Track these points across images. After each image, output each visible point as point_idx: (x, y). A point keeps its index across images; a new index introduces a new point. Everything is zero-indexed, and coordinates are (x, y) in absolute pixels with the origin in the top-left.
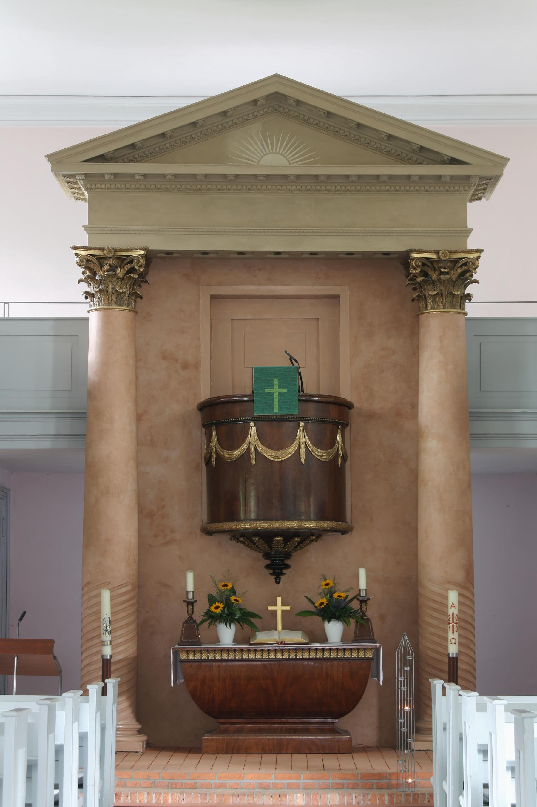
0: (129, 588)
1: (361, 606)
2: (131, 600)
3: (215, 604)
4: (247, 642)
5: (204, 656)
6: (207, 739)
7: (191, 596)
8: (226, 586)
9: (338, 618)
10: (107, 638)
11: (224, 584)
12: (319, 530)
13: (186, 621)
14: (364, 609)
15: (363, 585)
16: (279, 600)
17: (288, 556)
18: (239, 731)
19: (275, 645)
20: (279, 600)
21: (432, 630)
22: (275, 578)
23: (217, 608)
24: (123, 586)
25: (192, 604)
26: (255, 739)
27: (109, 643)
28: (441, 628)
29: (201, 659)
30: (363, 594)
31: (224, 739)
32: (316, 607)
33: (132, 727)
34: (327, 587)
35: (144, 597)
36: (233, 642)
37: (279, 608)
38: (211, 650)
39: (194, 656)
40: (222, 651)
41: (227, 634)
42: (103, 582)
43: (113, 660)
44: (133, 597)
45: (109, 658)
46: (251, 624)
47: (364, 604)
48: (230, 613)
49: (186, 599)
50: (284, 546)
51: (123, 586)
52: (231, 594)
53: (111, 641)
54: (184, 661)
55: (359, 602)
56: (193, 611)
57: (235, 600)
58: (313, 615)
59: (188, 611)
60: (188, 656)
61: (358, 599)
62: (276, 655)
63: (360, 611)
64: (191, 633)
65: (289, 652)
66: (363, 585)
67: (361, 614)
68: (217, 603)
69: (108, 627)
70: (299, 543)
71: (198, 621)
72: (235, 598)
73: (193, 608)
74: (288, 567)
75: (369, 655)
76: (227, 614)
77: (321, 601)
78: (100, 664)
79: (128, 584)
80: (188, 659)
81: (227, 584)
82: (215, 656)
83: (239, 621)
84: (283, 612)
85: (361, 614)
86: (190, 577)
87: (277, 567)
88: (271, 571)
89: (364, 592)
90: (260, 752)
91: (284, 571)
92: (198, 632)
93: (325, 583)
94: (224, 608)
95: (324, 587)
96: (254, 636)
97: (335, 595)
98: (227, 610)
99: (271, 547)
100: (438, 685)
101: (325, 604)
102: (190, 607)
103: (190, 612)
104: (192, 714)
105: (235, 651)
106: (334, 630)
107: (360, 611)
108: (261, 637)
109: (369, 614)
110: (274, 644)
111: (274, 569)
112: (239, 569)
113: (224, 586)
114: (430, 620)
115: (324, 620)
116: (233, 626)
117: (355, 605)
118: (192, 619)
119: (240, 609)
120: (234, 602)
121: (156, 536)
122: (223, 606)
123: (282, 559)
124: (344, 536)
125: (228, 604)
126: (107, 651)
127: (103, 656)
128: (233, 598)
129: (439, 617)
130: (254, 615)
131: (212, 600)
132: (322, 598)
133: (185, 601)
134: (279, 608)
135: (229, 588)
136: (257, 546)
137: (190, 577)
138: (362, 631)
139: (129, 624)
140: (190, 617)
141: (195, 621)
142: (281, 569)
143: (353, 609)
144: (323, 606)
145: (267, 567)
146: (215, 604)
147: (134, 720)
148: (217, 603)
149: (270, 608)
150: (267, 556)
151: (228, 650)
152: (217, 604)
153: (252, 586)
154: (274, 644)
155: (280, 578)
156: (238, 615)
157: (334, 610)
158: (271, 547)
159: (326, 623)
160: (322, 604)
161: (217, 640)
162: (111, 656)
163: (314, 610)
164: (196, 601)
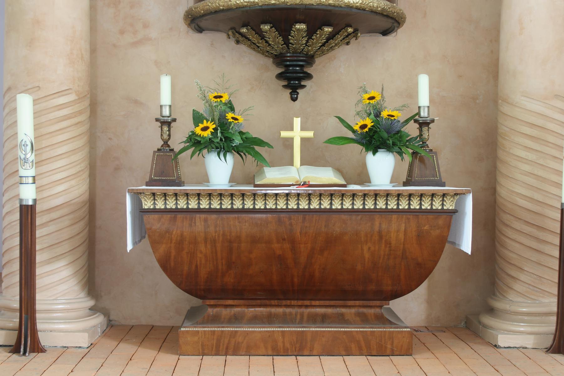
0: (72, 97)
1: (421, 131)
2: (76, 116)
3: (202, 123)
4: (250, 180)
5: (182, 204)
6: (187, 331)
7: (166, 112)
8: (221, 97)
9: (389, 148)
10: (28, 172)
11: (216, 94)
12: (364, 10)
13: (159, 150)
14: (425, 136)
15: (424, 100)
16: (297, 122)
17: (310, 59)
18: (235, 320)
19: (295, 188)
20: (297, 122)
21: (526, 168)
22: (291, 93)
23: (205, 129)
24: (60, 93)
25: (169, 124)
26: (260, 332)
27: (30, 180)
28: (542, 165)
29: (177, 208)
30: (424, 113)
31: (214, 331)
32: (354, 131)
33: (76, 306)
34: (372, 102)
35: (96, 108)
36: (230, 182)
37: (297, 134)
38: (193, 195)
39: (165, 204)
40: (376, 195)
41: (220, 170)
42: (29, 87)
43: (38, 208)
44: (80, 113)
45: (30, 203)
46: (257, 155)
47: (425, 129)
48: (225, 138)
49: (159, 117)
50: (307, 41)
51: (60, 93)
52: (228, 110)
53: (34, 177)
54: (149, 211)
55: (417, 126)
56: (169, 135)
57: (233, 118)
58: (350, 143)
59: (162, 135)
60: (154, 204)
61: (416, 121)
62: (298, 204)
63: (418, 139)
64: (165, 168)
65: (298, 199)
66: (424, 100)
67: (421, 143)
68: (205, 121)
69: (28, 156)
70: (331, 36)
71: (177, 149)
72: (233, 115)
73: (169, 130)
74: (309, 76)
75: (449, 205)
76: (221, 140)
77: (362, 123)
78: (17, 216)
79: (70, 91)
80: (155, 209)
81: (222, 95)
82: (199, 203)
83: (238, 150)
84: (304, 141)
85: (421, 143)
86: (166, 82)
87: (293, 75)
88: (285, 83)
89: (426, 109)
90: (270, 353)
91: (303, 83)
92: (176, 167)
93: (367, 96)
94: (215, 129)
95: (368, 101)
96: (260, 172)
97: (384, 114)
98: (222, 133)
99: (287, 42)
100: (470, 253)
101: (369, 126)
102: (166, 128)
103: (165, 137)
104: (163, 297)
105: (232, 195)
106: (382, 168)
107: (418, 139)
108: (272, 175)
109: (431, 144)
110: (293, 185)
111: (289, 79)
112: (236, 75)
113: (216, 97)
114: (523, 154)
115: (367, 150)
116: (229, 156)
117: (412, 130)
118: (169, 146)
119: (241, 133)
120: (232, 120)
121: (122, 32)
122: (214, 126)
123: (301, 63)
124: (385, 37)
125: (223, 124)
126: (28, 194)
127: (21, 200)
128: (230, 116)
129: (539, 149)
130: (260, 142)
131: (198, 118)
132: (364, 119)
133: (157, 120)
134: (297, 134)
135: (223, 100)
136: (267, 42)
137: (166, 82)
138: (420, 164)
139: (73, 152)
140: (166, 143)
141: (172, 150)
142: (300, 79)
143: (409, 136)
144: (367, 130)
145: (280, 76)
146: (202, 123)
147: (82, 295)
148: (205, 121)
149: (284, 134)
150: (279, 59)
151: (221, 195)
152: (205, 124)
153: (257, 101)
154: (293, 185)
155: (298, 93)
156: (237, 141)
157: (378, 136)
158: (287, 42)
159: (370, 156)
160: (363, 127)
161: (206, 179)
162: (35, 201)
163: (351, 135)
164: (174, 120)
